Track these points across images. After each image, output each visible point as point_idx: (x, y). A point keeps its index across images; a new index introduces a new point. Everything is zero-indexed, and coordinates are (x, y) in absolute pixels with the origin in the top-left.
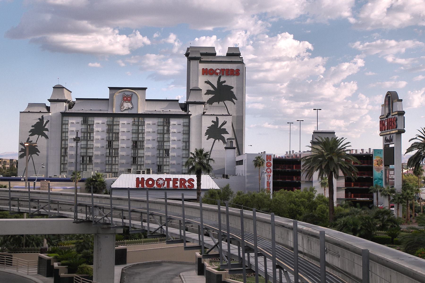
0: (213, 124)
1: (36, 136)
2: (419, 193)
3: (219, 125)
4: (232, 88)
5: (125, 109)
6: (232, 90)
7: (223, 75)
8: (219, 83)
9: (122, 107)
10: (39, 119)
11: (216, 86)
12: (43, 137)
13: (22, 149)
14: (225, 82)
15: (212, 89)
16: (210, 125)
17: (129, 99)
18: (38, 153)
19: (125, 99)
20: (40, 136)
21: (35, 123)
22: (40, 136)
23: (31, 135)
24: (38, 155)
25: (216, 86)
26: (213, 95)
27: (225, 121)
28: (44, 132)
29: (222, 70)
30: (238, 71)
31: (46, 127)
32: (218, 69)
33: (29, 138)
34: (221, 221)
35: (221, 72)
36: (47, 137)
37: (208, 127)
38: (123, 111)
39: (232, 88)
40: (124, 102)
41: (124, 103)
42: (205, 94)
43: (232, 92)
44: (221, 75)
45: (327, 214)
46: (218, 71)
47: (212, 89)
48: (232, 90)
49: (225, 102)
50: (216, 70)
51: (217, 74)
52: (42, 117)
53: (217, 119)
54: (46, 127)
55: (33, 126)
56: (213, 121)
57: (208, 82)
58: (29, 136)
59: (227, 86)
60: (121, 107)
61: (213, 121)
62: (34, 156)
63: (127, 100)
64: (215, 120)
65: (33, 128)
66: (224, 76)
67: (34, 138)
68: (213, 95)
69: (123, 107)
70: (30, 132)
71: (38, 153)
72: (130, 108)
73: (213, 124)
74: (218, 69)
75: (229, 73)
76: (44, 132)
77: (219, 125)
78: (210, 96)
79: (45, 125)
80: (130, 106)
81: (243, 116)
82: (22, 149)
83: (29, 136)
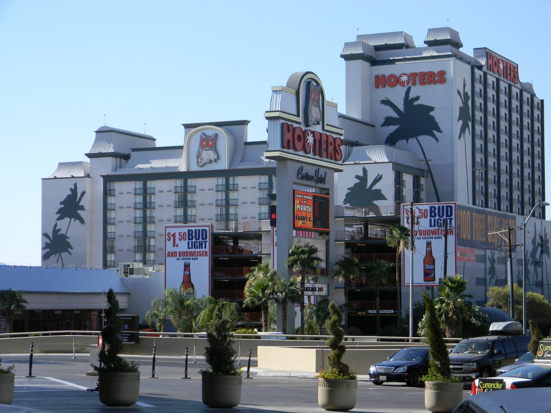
1: (67, 219)
3: (369, 184)
4: (432, 109)
5: (204, 162)
6: (432, 114)
7: (414, 84)
8: (408, 102)
9: (199, 159)
11: (401, 107)
12: (77, 221)
13: (47, 244)
14: (417, 98)
15: (394, 115)
16: (352, 185)
17: (210, 143)
18: (69, 250)
19: (204, 143)
20: (73, 219)
21: (63, 197)
22: (73, 219)
23: (59, 219)
24: (70, 253)
25: (401, 107)
27: (379, 175)
29: (413, 77)
30: (441, 75)
31: (81, 204)
32: (405, 74)
33: (56, 225)
34: (243, 359)
36: (82, 221)
37: (349, 189)
38: (204, 164)
39: (432, 109)
40: (202, 150)
41: (204, 151)
42: (383, 125)
43: (433, 118)
44: (410, 85)
45: (256, 333)
47: (394, 115)
48: (432, 114)
49: (419, 138)
50: (401, 76)
51: (402, 84)
52: (75, 185)
53: (365, 171)
54: (81, 204)
55: (61, 203)
56: (357, 177)
57: (387, 102)
58: (57, 220)
59: (422, 106)
60: (197, 159)
61: (357, 177)
62: (64, 255)
63: (207, 145)
66: (427, 84)
67: (63, 224)
68: (396, 127)
69: (201, 159)
70: (57, 213)
74: (405, 74)
75: (426, 80)
77: (369, 184)
78: (392, 128)
79: (80, 200)
80: (213, 156)
81: (453, 164)
82: (47, 244)
83: (57, 220)
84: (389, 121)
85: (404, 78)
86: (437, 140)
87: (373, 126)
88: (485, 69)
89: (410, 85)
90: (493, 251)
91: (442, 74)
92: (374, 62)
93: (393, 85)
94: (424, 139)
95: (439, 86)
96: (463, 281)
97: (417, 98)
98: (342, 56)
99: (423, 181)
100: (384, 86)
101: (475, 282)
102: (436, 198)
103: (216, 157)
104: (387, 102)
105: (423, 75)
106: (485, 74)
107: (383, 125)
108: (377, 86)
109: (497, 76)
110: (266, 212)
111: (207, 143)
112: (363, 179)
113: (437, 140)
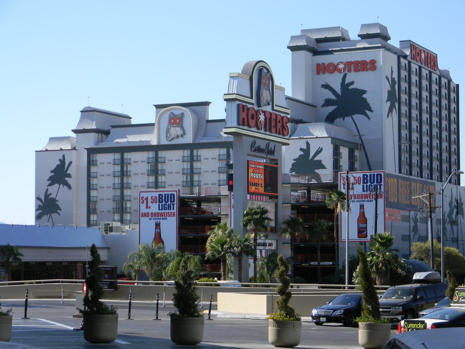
0: (302, 153)
1: (56, 185)
2: (264, 255)
3: (311, 155)
4: (364, 92)
5: (172, 137)
6: (364, 96)
7: (350, 71)
8: (344, 86)
9: (168, 135)
10: (60, 160)
11: (339, 91)
12: (65, 187)
13: (39, 206)
14: (352, 83)
15: (333, 97)
16: (297, 157)
17: (178, 121)
18: (59, 211)
19: (172, 121)
20: (62, 185)
21: (53, 167)
22: (62, 185)
23: (50, 185)
24: (59, 214)
25: (339, 91)
26: (334, 107)
27: (319, 148)
28: (67, 179)
29: (348, 65)
30: (372, 63)
31: (68, 172)
32: (341, 63)
33: (47, 190)
35: (347, 66)
36: (69, 187)
37: (294, 160)
38: (173, 139)
39: (364, 92)
40: (171, 127)
41: (172, 127)
42: (323, 106)
43: (365, 100)
44: (346, 71)
46: (341, 66)
47: (333, 97)
48: (364, 96)
49: (354, 116)
50: (338, 64)
51: (340, 71)
52: (64, 156)
53: (308, 144)
54: (68, 172)
55: (52, 172)
56: (301, 150)
57: (326, 86)
58: (48, 186)
59: (356, 90)
60: (167, 135)
61: (301, 150)
62: (54, 215)
63: (175, 122)
64: (305, 147)
65: (53, 174)
66: (360, 71)
67: (53, 189)
68: (334, 107)
69: (170, 135)
70: (48, 180)
71: (59, 211)
72: (180, 135)
73: (302, 153)
74: (341, 63)
75: (359, 68)
76: (67, 179)
77: (311, 155)
78: (331, 109)
79: (68, 169)
80: (180, 132)
81: (382, 138)
82: (39, 206)
83: (48, 186)
84: (328, 102)
85: (341, 66)
86: (369, 118)
87: (315, 107)
88: (409, 58)
89: (346, 71)
90: (416, 212)
91: (373, 62)
92: (315, 52)
93: (331, 72)
94: (358, 117)
95: (370, 73)
96: (391, 238)
97: (352, 83)
98: (289, 47)
99: (357, 153)
100: (324, 73)
101: (401, 238)
102: (368, 167)
103: (182, 133)
104: (326, 86)
105: (357, 63)
106: (409, 63)
107: (323, 106)
108: (318, 73)
109: (419, 64)
110: (225, 179)
111: (175, 121)
112: (306, 151)
113: (369, 118)
